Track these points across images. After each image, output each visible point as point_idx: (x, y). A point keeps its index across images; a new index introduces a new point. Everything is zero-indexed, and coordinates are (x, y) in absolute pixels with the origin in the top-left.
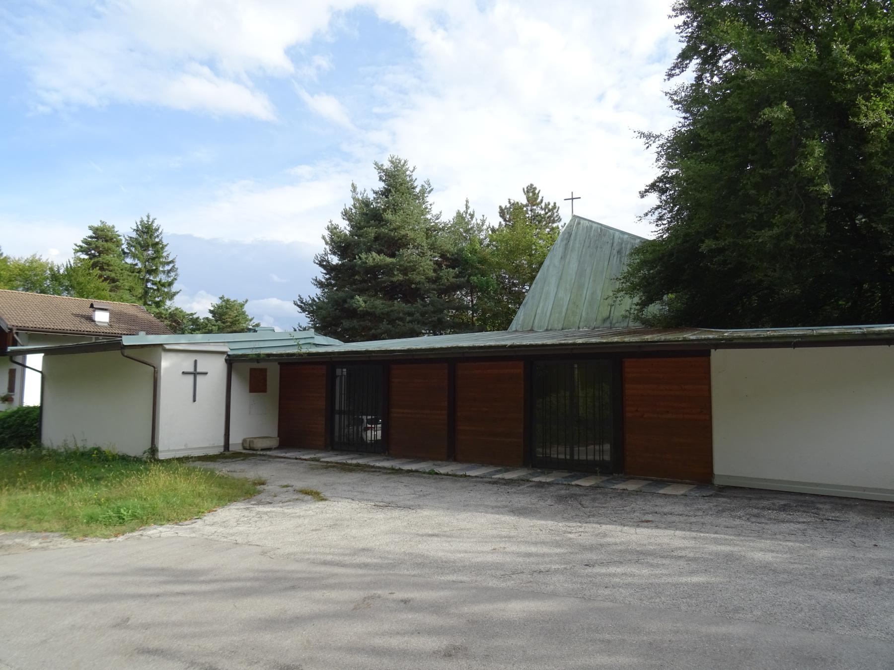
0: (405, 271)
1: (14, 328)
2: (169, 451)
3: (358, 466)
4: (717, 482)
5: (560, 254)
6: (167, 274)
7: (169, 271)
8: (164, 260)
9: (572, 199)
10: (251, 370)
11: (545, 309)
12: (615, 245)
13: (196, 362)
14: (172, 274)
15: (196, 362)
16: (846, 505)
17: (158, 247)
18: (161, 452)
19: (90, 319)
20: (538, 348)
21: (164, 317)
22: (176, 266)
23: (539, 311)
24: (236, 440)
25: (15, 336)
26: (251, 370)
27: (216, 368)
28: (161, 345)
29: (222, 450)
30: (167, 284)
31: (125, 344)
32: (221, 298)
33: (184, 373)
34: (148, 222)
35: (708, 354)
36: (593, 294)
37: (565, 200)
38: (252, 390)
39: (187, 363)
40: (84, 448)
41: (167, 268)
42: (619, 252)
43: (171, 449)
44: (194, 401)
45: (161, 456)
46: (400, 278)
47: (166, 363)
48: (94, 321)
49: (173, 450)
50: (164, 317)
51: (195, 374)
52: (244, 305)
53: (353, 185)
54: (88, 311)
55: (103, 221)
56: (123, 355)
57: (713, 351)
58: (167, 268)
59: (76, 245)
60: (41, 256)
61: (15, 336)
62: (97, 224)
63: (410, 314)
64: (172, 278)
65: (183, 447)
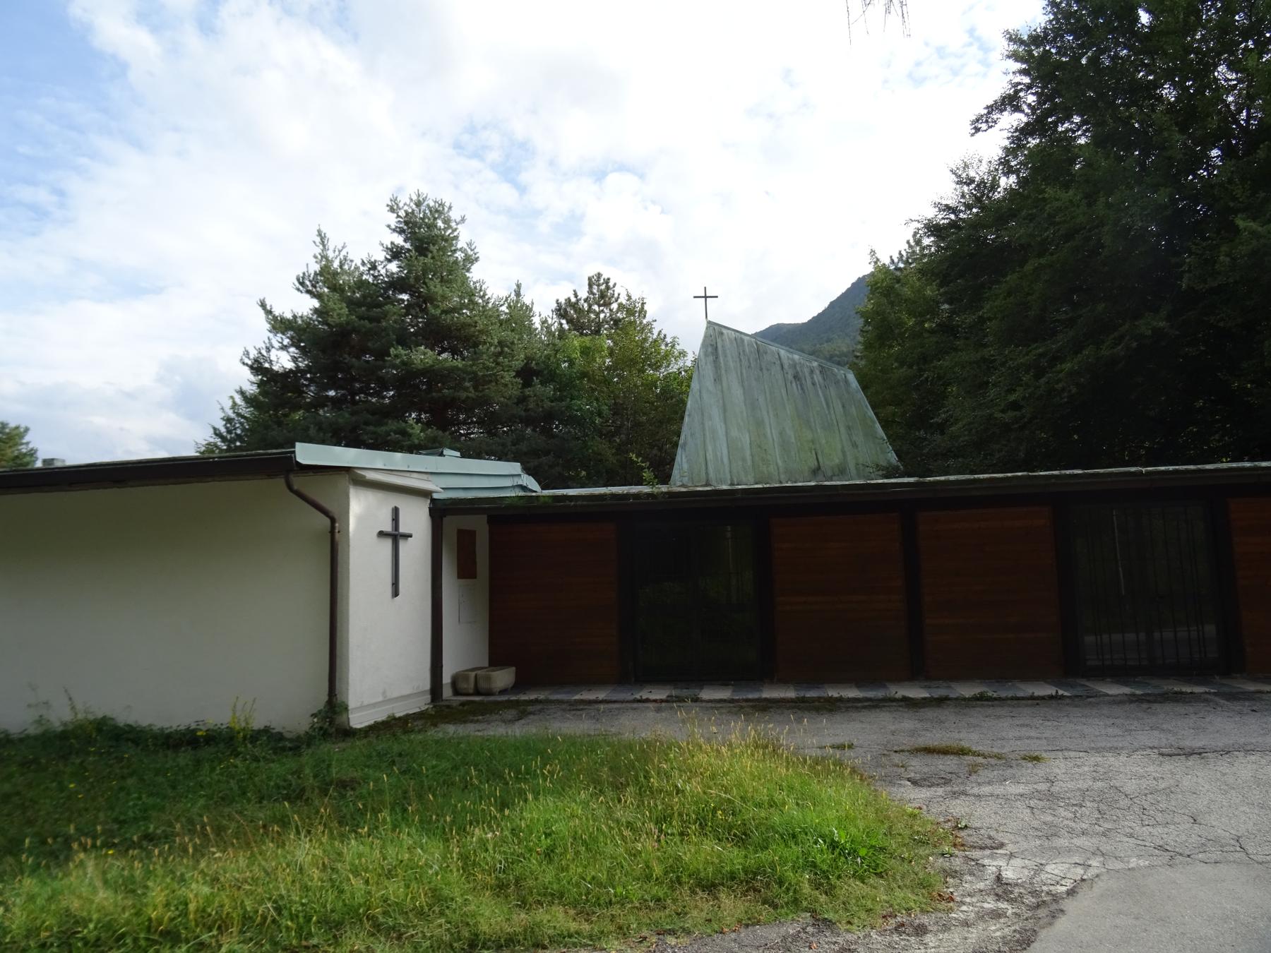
0: (478, 382)
3: (803, 702)
5: (711, 375)
9: (706, 297)
11: (719, 454)
12: (786, 367)
13: (396, 511)
15: (396, 511)
16: (849, 707)
23: (710, 456)
36: (781, 434)
37: (695, 297)
40: (246, 721)
42: (796, 377)
43: (366, 703)
46: (470, 395)
53: (320, 233)
56: (290, 488)
65: (381, 699)
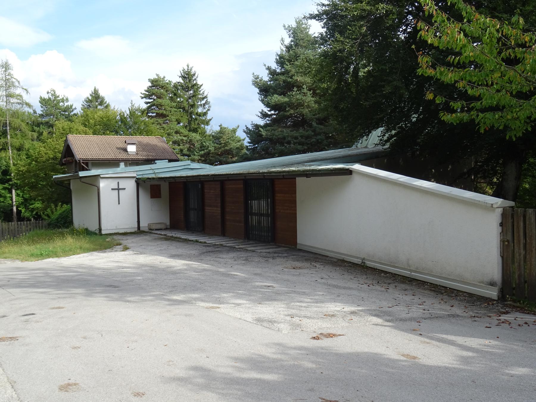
1: (81, 160)
2: (107, 230)
4: (298, 247)
6: (204, 106)
7: (204, 105)
8: (201, 96)
10: (151, 186)
13: (118, 182)
14: (207, 106)
15: (118, 182)
17: (196, 87)
18: (104, 230)
19: (125, 150)
20: (220, 176)
21: (185, 142)
22: (208, 101)
24: (144, 224)
25: (82, 164)
26: (151, 186)
27: (130, 186)
28: (99, 175)
29: (136, 229)
30: (202, 114)
31: (80, 176)
32: (220, 126)
33: (112, 189)
34: (188, 69)
35: (295, 178)
38: (151, 198)
39: (113, 184)
41: (203, 102)
43: (108, 229)
44: (119, 204)
45: (103, 232)
47: (103, 184)
48: (127, 152)
49: (110, 230)
50: (185, 142)
51: (118, 189)
52: (236, 129)
54: (122, 145)
55: (157, 74)
57: (297, 178)
58: (203, 102)
59: (141, 93)
60: (115, 106)
61: (82, 164)
62: (153, 77)
63: (296, 138)
64: (207, 109)
65: (115, 228)
